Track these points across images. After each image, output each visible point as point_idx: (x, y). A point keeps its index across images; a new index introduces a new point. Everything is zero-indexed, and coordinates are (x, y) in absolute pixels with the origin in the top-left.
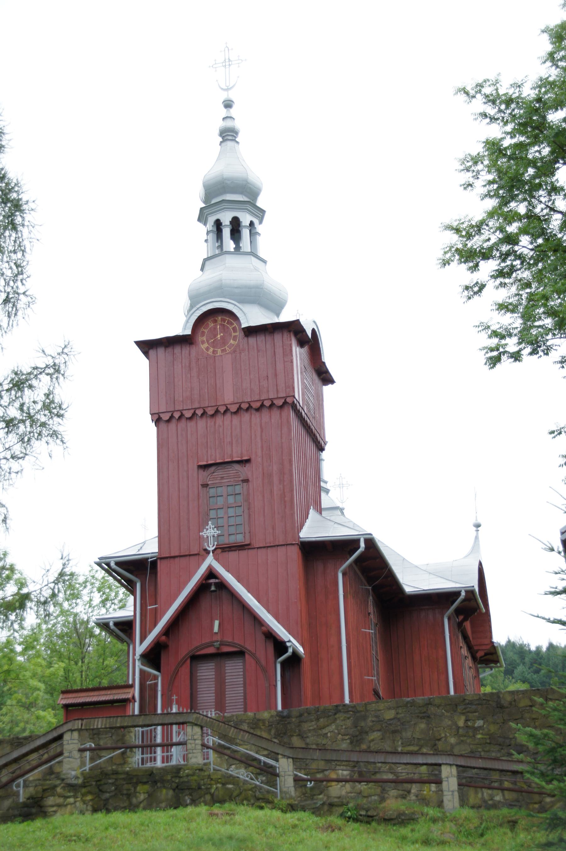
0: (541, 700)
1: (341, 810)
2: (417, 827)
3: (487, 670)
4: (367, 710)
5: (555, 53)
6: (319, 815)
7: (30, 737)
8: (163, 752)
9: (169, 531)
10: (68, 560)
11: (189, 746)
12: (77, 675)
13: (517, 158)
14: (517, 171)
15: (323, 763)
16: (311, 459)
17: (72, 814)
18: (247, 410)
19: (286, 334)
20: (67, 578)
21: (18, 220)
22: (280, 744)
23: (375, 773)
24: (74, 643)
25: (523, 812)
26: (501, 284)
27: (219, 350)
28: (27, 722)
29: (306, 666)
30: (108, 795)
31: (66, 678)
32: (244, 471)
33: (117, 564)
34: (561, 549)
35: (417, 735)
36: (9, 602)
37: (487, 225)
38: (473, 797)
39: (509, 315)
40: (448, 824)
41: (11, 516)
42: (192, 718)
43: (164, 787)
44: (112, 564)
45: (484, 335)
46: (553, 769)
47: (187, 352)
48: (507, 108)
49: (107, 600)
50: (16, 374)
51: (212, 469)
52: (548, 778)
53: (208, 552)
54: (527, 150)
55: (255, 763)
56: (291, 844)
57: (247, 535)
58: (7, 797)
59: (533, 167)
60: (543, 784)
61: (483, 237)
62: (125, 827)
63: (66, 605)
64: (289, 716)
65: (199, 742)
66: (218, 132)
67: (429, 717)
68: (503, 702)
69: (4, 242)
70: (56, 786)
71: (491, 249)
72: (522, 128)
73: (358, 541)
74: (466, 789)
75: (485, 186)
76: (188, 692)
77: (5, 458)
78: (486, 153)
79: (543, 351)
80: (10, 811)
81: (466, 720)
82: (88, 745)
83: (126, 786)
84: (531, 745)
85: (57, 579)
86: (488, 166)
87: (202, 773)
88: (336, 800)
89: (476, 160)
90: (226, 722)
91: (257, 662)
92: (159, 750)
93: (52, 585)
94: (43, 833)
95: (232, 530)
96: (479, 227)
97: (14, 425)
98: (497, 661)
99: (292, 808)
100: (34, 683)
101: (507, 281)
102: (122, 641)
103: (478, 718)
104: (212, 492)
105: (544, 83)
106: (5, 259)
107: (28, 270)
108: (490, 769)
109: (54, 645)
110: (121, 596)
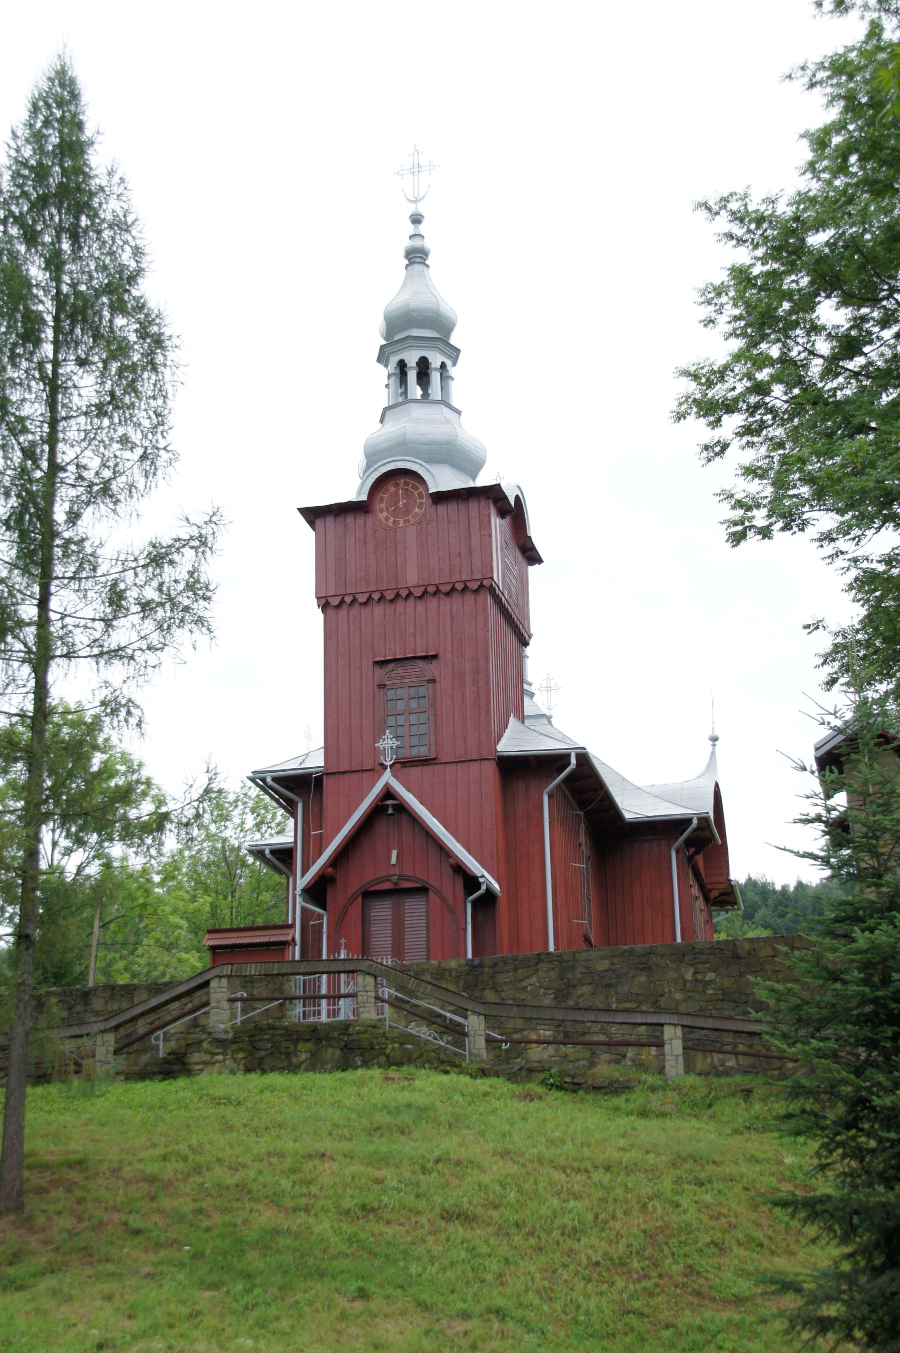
0: (785, 949)
1: (542, 1076)
2: (633, 1097)
3: (722, 913)
4: (575, 960)
5: (816, 162)
6: (516, 1082)
7: (171, 983)
8: (329, 1005)
9: (338, 740)
10: (216, 774)
11: (360, 999)
12: (227, 912)
13: (769, 289)
14: (769, 305)
15: (521, 1021)
16: (512, 656)
17: (221, 1073)
18: (435, 594)
19: (483, 502)
20: (213, 796)
21: (159, 358)
22: (471, 998)
23: (584, 1034)
24: (223, 874)
25: (760, 1080)
26: (748, 443)
27: (401, 521)
28: (167, 966)
29: (503, 906)
30: (263, 1053)
31: (213, 915)
32: (430, 669)
33: (274, 779)
34: (815, 768)
35: (636, 990)
36: (145, 822)
37: (732, 371)
38: (701, 1063)
39: (757, 481)
40: (669, 1094)
41: (146, 719)
42: (364, 965)
43: (330, 1046)
44: (269, 780)
45: (726, 505)
46: (797, 1030)
47: (362, 522)
48: (757, 228)
49: (262, 822)
50: (154, 546)
51: (391, 666)
52: (791, 1041)
53: (385, 768)
54: (782, 280)
55: (439, 1020)
56: (481, 1114)
57: (433, 747)
58: (144, 1051)
59: (788, 301)
60: (785, 1046)
61: (727, 386)
62: (283, 1091)
63: (213, 828)
64: (480, 966)
65: (372, 994)
66: (403, 253)
67: (650, 968)
68: (739, 951)
69: (142, 386)
70: (201, 1041)
71: (736, 400)
72: (775, 253)
73: (569, 756)
74: (693, 1052)
75: (730, 322)
76: (360, 935)
77: (140, 649)
78: (732, 283)
79: (798, 526)
80: (149, 1068)
81: (695, 973)
82: (239, 995)
83: (284, 1044)
84: (772, 1002)
85: (202, 796)
86: (733, 299)
87: (376, 1031)
88: (536, 1064)
89: (719, 291)
90: (404, 971)
91: (444, 900)
92: (324, 1002)
93: (196, 804)
94: (187, 1094)
95: (415, 741)
96: (722, 374)
97: (151, 609)
98: (734, 903)
99: (483, 1073)
100: (175, 919)
101: (755, 439)
102: (280, 872)
103: (710, 970)
104: (390, 694)
105: (804, 199)
106: (143, 407)
107: (171, 420)
108: (723, 1030)
109: (199, 875)
110: (279, 818)
